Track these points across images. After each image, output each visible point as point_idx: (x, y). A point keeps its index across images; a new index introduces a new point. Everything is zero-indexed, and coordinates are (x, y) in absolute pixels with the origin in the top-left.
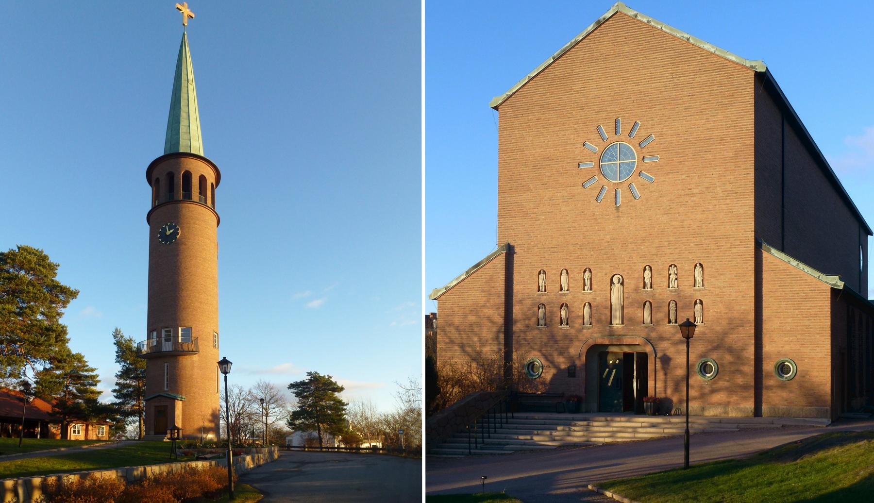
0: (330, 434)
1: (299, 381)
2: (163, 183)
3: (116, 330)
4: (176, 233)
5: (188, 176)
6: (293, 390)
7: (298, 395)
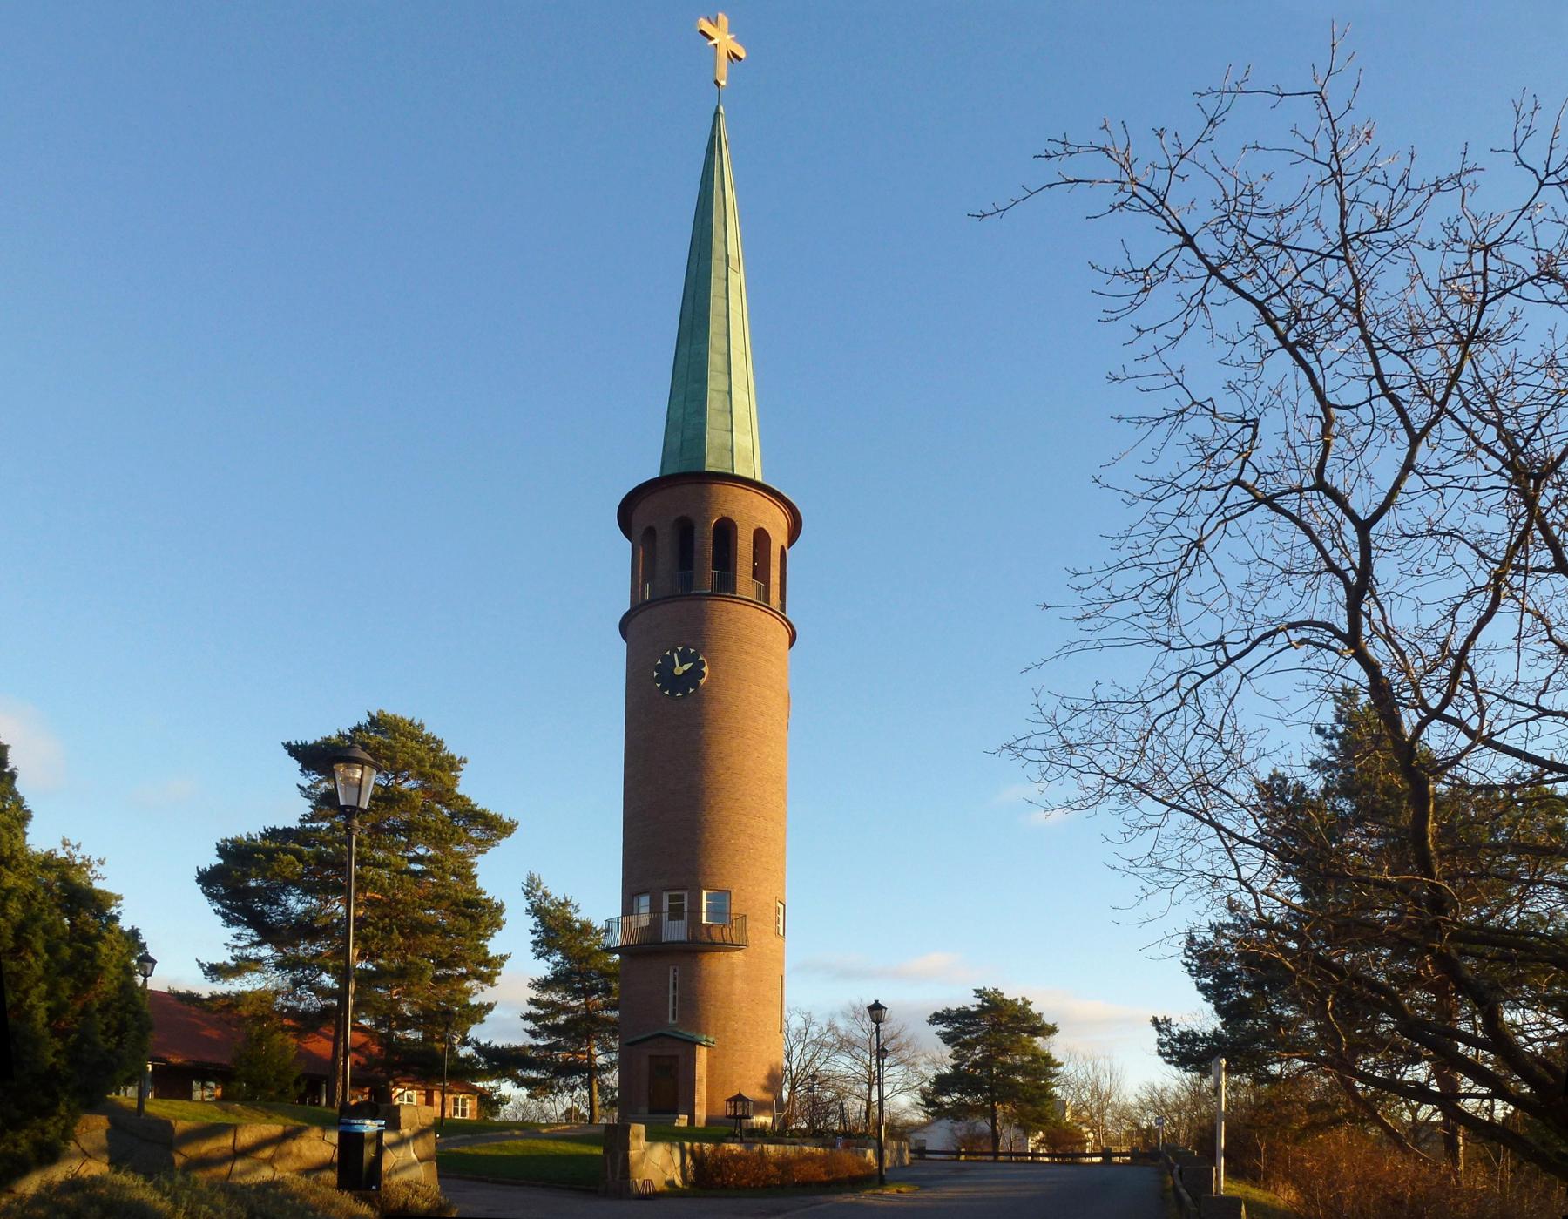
0: (1019, 1126)
1: (954, 1008)
2: (666, 542)
3: (531, 879)
4: (696, 672)
5: (726, 531)
6: (941, 1028)
7: (948, 1039)
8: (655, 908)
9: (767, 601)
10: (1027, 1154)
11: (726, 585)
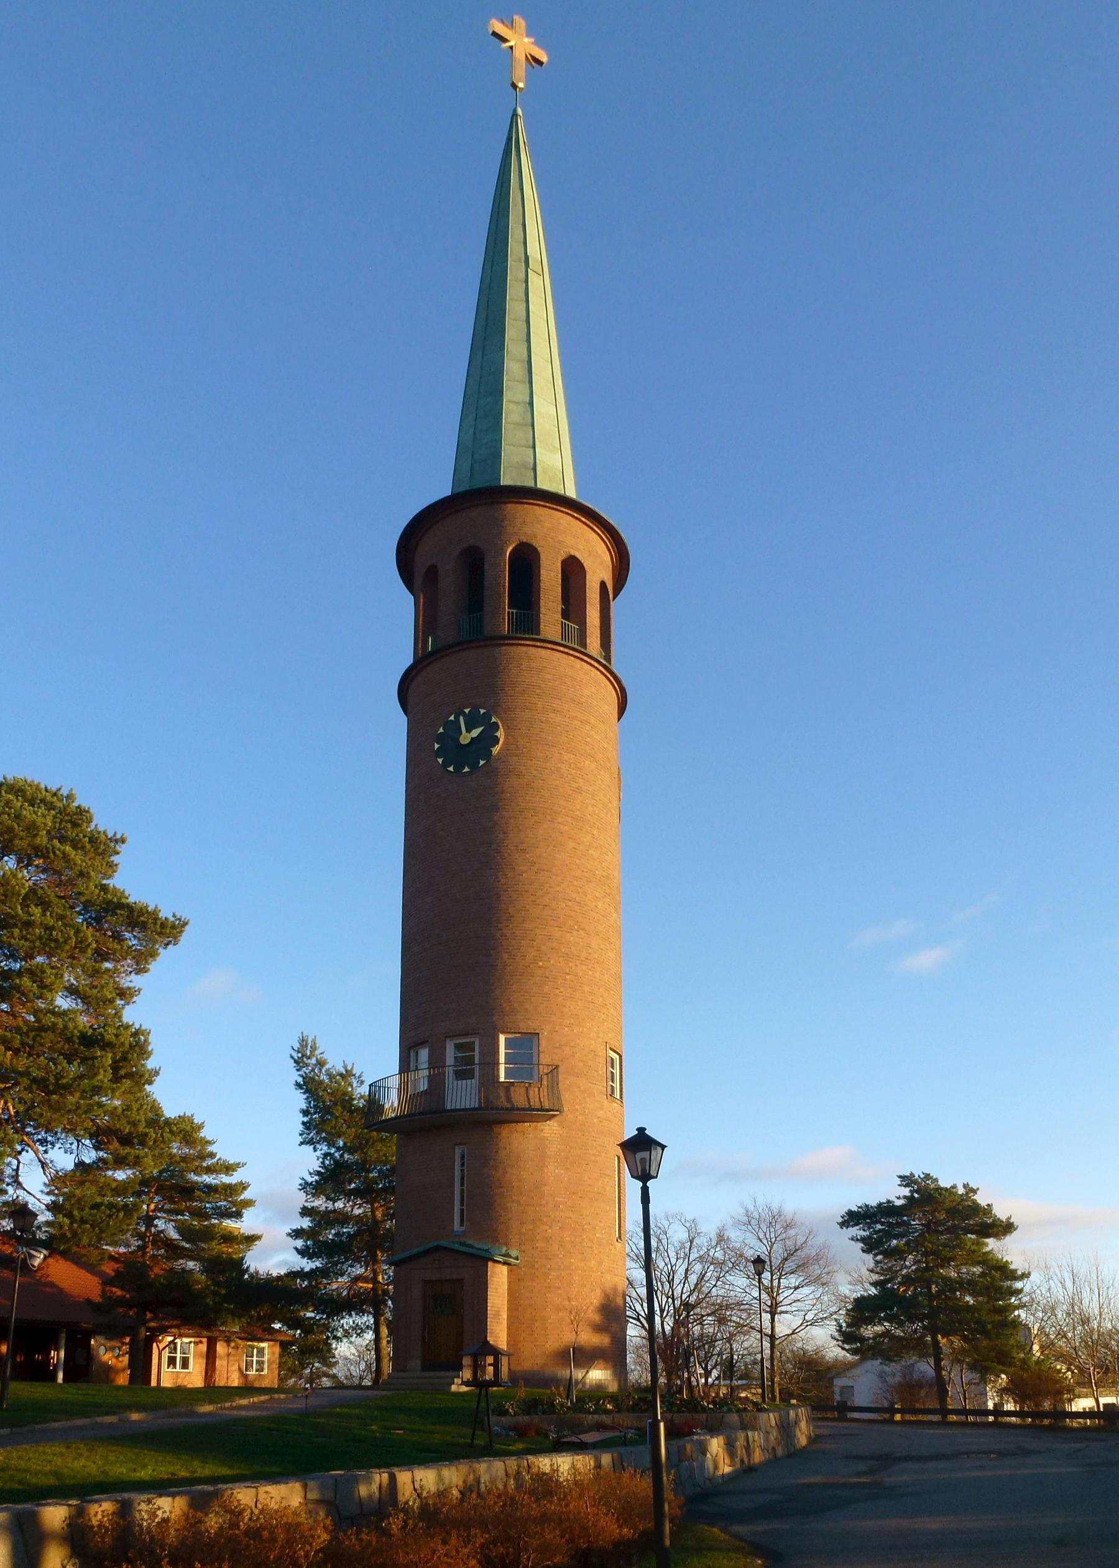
0: (973, 1367)
1: (873, 1202)
3: (303, 1042)
5: (526, 561)
6: (856, 1231)
7: (870, 1245)
8: (437, 1062)
9: (584, 645)
10: (988, 1413)
11: (527, 623)
